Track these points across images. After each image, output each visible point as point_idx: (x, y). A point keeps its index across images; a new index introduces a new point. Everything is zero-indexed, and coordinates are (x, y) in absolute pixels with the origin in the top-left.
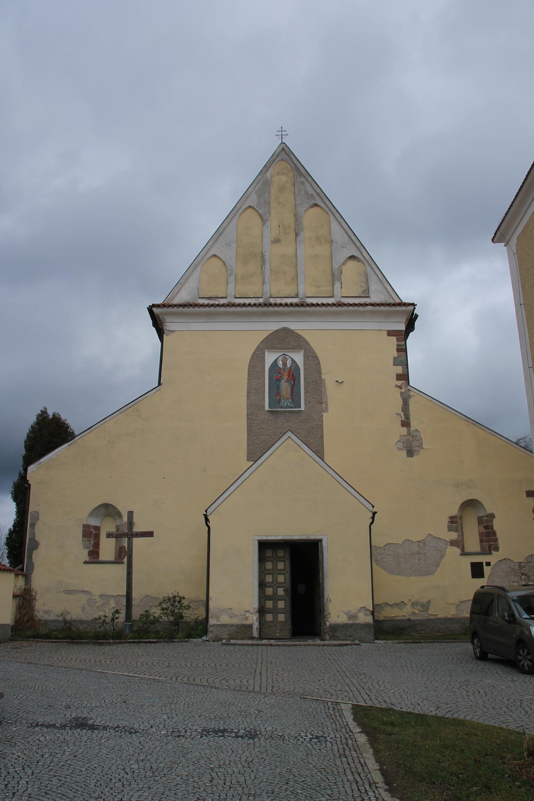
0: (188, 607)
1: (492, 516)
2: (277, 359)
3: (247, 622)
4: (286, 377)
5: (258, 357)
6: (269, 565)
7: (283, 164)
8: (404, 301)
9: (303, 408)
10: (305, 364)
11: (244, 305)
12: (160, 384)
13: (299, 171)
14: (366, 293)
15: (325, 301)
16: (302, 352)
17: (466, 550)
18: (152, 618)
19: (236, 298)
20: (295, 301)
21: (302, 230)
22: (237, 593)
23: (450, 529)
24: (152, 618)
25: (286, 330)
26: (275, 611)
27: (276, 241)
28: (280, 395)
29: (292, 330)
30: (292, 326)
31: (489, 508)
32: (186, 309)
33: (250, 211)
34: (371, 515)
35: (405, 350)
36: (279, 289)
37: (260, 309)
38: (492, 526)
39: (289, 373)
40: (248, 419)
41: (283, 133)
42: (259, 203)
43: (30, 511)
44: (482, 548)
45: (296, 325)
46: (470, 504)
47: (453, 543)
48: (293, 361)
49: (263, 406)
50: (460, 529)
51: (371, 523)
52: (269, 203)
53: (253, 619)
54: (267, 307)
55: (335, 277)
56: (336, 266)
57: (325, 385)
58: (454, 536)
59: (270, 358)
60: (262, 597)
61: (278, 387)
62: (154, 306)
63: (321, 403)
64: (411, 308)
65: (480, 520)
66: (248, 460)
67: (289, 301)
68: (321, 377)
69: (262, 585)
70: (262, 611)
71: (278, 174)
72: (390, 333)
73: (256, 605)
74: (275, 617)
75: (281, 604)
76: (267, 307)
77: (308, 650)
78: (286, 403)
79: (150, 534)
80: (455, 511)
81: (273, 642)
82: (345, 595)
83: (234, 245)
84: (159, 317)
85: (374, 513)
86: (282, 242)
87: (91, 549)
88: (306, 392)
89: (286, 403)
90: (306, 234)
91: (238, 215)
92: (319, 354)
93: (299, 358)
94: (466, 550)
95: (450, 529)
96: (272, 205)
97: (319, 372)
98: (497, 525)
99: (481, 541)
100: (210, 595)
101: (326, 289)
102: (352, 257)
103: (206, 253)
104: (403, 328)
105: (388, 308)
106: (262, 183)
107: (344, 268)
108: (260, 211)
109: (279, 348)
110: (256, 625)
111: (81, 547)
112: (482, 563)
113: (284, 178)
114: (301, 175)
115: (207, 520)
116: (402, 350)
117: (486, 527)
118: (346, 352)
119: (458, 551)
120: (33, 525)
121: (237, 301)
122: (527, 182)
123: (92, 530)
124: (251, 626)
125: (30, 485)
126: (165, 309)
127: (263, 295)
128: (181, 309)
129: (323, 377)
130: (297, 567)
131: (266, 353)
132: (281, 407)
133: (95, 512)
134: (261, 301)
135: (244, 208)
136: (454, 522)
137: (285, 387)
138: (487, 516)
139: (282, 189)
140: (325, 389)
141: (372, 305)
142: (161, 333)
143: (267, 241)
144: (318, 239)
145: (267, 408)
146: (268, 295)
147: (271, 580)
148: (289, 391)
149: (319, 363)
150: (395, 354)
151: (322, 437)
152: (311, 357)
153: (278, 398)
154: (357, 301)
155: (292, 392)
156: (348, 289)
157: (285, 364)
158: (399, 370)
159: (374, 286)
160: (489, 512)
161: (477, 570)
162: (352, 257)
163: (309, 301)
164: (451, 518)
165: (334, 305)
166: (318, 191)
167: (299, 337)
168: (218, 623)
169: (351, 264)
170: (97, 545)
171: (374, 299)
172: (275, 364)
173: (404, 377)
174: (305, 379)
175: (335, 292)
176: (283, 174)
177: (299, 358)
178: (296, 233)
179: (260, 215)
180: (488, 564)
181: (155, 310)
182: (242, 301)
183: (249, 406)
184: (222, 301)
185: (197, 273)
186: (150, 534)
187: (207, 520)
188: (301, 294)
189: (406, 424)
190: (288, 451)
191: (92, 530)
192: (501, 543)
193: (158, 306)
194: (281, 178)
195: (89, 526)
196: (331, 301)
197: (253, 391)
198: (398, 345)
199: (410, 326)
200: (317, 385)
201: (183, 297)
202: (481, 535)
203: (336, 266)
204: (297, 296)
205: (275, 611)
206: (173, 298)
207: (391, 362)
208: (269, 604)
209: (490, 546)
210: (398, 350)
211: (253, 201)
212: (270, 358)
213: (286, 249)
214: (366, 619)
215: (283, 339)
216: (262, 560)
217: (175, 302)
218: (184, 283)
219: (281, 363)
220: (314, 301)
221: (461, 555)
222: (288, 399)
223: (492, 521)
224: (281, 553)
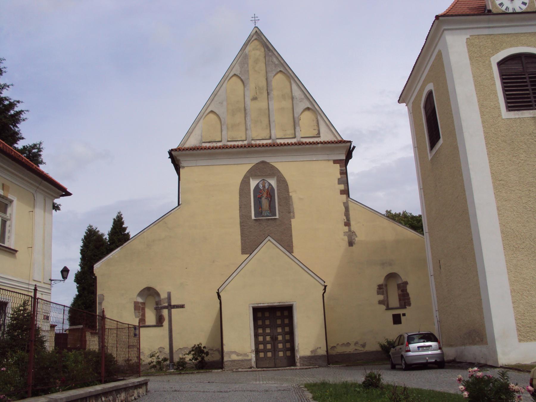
0: (207, 354)
1: (406, 283)
2: (258, 183)
3: (249, 358)
4: (265, 195)
5: (245, 183)
6: (260, 323)
7: (256, 42)
8: (344, 139)
9: (277, 217)
10: (278, 186)
11: (234, 147)
12: (179, 204)
14: (318, 135)
15: (290, 141)
16: (276, 178)
17: (390, 306)
18: (188, 358)
19: (228, 141)
20: (269, 141)
21: (272, 90)
22: (240, 340)
23: (378, 293)
24: (188, 358)
25: (263, 162)
27: (255, 99)
28: (261, 208)
29: (268, 163)
30: (268, 160)
31: (404, 278)
32: (195, 152)
33: (234, 78)
34: (323, 287)
35: (346, 173)
36: (258, 134)
37: (245, 149)
38: (406, 290)
39: (267, 192)
40: (241, 226)
41: (256, 19)
42: (241, 72)
43: (98, 294)
44: (400, 304)
46: (391, 276)
47: (380, 302)
48: (270, 184)
49: (251, 216)
50: (385, 293)
51: (324, 293)
52: (248, 71)
53: (253, 356)
54: (250, 149)
55: (295, 123)
57: (292, 200)
58: (381, 297)
59: (253, 184)
60: (257, 343)
61: (260, 203)
62: (172, 150)
63: (290, 213)
64: (349, 144)
65: (399, 286)
66: (243, 252)
67: (265, 142)
68: (289, 195)
69: (256, 335)
70: (257, 351)
71: (254, 49)
72: (335, 162)
73: (253, 348)
74: (265, 355)
78: (266, 215)
79: (182, 306)
80: (381, 281)
81: (265, 369)
82: (308, 337)
83: (225, 103)
84: (176, 157)
85: (325, 286)
86: (259, 99)
87: (140, 317)
88: (280, 205)
89: (266, 215)
90: (275, 93)
91: (227, 81)
92: (287, 178)
93: (273, 182)
94: (390, 306)
95: (378, 293)
96: (250, 72)
97: (288, 191)
98: (410, 289)
99: (400, 300)
100: (224, 342)
101: (265, 134)
102: (308, 109)
103: (206, 110)
104: (344, 158)
105: (333, 145)
106: (243, 57)
107: (302, 117)
108: (242, 78)
109: (259, 176)
110: (254, 359)
111: (134, 317)
112: (400, 314)
113: (258, 53)
114: (269, 50)
115: (219, 297)
116: (344, 173)
117: (402, 291)
118: (305, 179)
119: (384, 307)
120: (100, 304)
121: (230, 144)
122: (414, 71)
123: (140, 305)
124: (250, 360)
125: (96, 277)
126: (180, 152)
127: (246, 138)
128: (191, 152)
129: (291, 194)
130: (274, 320)
131: (251, 180)
132: (263, 217)
133: (141, 294)
134: (245, 143)
135: (231, 75)
136: (382, 289)
137: (265, 203)
138: (403, 283)
139: (256, 61)
140: (292, 202)
141: (321, 143)
142: (178, 168)
143: (248, 100)
144: (283, 97)
145: (253, 217)
146: (251, 139)
147: (266, 315)
148: (268, 205)
149: (287, 185)
150: (339, 176)
151: (291, 236)
152: (282, 182)
153: (260, 210)
154: (311, 140)
155: (270, 206)
156: (305, 131)
157: (264, 187)
158: (342, 187)
159: (323, 129)
160: (404, 280)
161: (397, 320)
162: (308, 109)
163: (279, 141)
164: (380, 287)
165: (296, 144)
166: (282, 62)
167: (273, 167)
168: (230, 359)
169: (307, 114)
170: (143, 315)
171: (322, 139)
172: (257, 185)
173: (346, 192)
174: (278, 196)
175: (297, 134)
176: (257, 49)
178: (268, 93)
179: (242, 80)
180: (404, 315)
181: (173, 153)
182: (232, 143)
183: (241, 216)
184: (219, 144)
185: (200, 124)
186: (182, 306)
187: (219, 297)
188: (273, 136)
189: (347, 224)
190: (269, 249)
191: (140, 305)
192: (412, 301)
193: (175, 150)
194: (256, 52)
195: (138, 303)
196: (293, 141)
197: (243, 206)
198: (341, 170)
199: (349, 156)
200: (286, 200)
201: (192, 142)
202: (399, 295)
203: (296, 115)
204: (270, 138)
206: (185, 144)
207: (337, 182)
208: (261, 347)
209: (405, 303)
210: (341, 173)
211: (237, 70)
212: (253, 184)
213: (262, 104)
214: (322, 351)
218: (192, 132)
219: (261, 186)
220: (282, 141)
221: (386, 309)
223: (406, 287)
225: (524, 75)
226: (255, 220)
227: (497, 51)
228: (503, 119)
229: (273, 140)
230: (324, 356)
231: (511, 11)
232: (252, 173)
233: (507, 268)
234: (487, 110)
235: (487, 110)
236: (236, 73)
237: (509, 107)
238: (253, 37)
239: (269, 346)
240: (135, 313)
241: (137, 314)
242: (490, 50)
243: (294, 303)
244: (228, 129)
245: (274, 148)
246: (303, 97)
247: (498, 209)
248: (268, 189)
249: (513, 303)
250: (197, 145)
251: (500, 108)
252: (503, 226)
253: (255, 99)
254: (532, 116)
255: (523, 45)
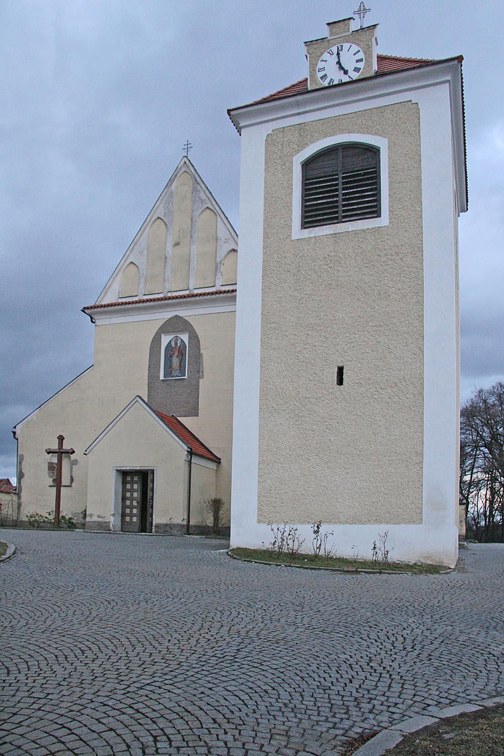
2: (171, 340)
3: (108, 520)
4: (176, 354)
5: (156, 340)
13: (197, 181)
25: (177, 317)
26: (131, 515)
27: (177, 244)
30: (181, 313)
36: (173, 286)
39: (179, 350)
45: (183, 313)
48: (182, 340)
54: (165, 301)
56: (218, 260)
59: (165, 340)
61: (171, 361)
62: (84, 308)
63: (199, 372)
68: (200, 352)
69: (124, 498)
75: (135, 511)
76: (165, 301)
77: (143, 537)
83: (145, 252)
91: (149, 226)
93: (185, 337)
103: (125, 262)
108: (165, 221)
109: (169, 332)
123: (55, 465)
129: (201, 352)
132: (172, 377)
137: (175, 361)
145: (162, 377)
152: (194, 337)
157: (176, 344)
177: (185, 337)
179: (165, 224)
183: (150, 377)
188: (191, 287)
191: (55, 465)
193: (88, 308)
194: (182, 187)
200: (197, 357)
205: (131, 515)
215: (176, 325)
216: (124, 483)
217: (103, 303)
219: (174, 343)
222: (177, 370)
224: (136, 478)
225: (337, 175)
226: (163, 380)
227: (303, 146)
228: (293, 241)
229: (190, 291)
230: (183, 526)
231: (336, 82)
232: (166, 328)
233: (260, 434)
234: (274, 231)
235: (274, 231)
236: (160, 217)
237: (306, 223)
238: (181, 169)
239: (128, 511)
240: (49, 473)
241: (51, 474)
242: (295, 146)
243: (155, 469)
244: (146, 280)
245: (190, 298)
246: (228, 236)
247: (261, 360)
248: (180, 347)
249: (259, 476)
250: (114, 302)
251: (291, 226)
252: (264, 381)
253: (177, 244)
254: (332, 232)
255: (342, 132)
